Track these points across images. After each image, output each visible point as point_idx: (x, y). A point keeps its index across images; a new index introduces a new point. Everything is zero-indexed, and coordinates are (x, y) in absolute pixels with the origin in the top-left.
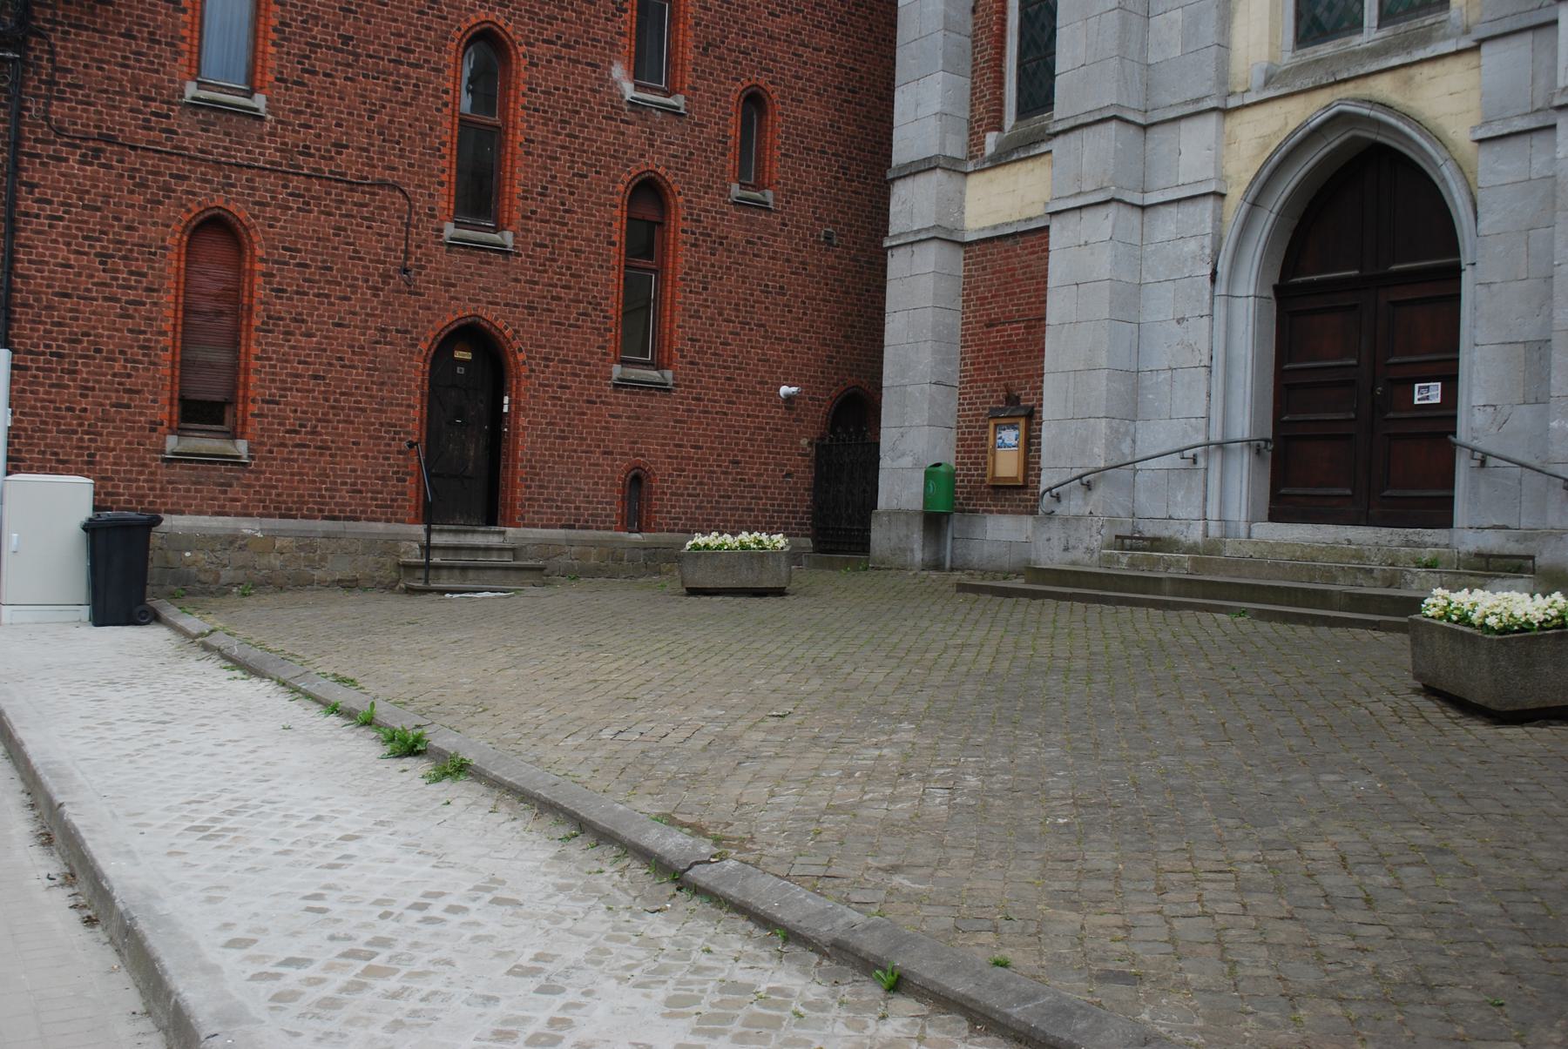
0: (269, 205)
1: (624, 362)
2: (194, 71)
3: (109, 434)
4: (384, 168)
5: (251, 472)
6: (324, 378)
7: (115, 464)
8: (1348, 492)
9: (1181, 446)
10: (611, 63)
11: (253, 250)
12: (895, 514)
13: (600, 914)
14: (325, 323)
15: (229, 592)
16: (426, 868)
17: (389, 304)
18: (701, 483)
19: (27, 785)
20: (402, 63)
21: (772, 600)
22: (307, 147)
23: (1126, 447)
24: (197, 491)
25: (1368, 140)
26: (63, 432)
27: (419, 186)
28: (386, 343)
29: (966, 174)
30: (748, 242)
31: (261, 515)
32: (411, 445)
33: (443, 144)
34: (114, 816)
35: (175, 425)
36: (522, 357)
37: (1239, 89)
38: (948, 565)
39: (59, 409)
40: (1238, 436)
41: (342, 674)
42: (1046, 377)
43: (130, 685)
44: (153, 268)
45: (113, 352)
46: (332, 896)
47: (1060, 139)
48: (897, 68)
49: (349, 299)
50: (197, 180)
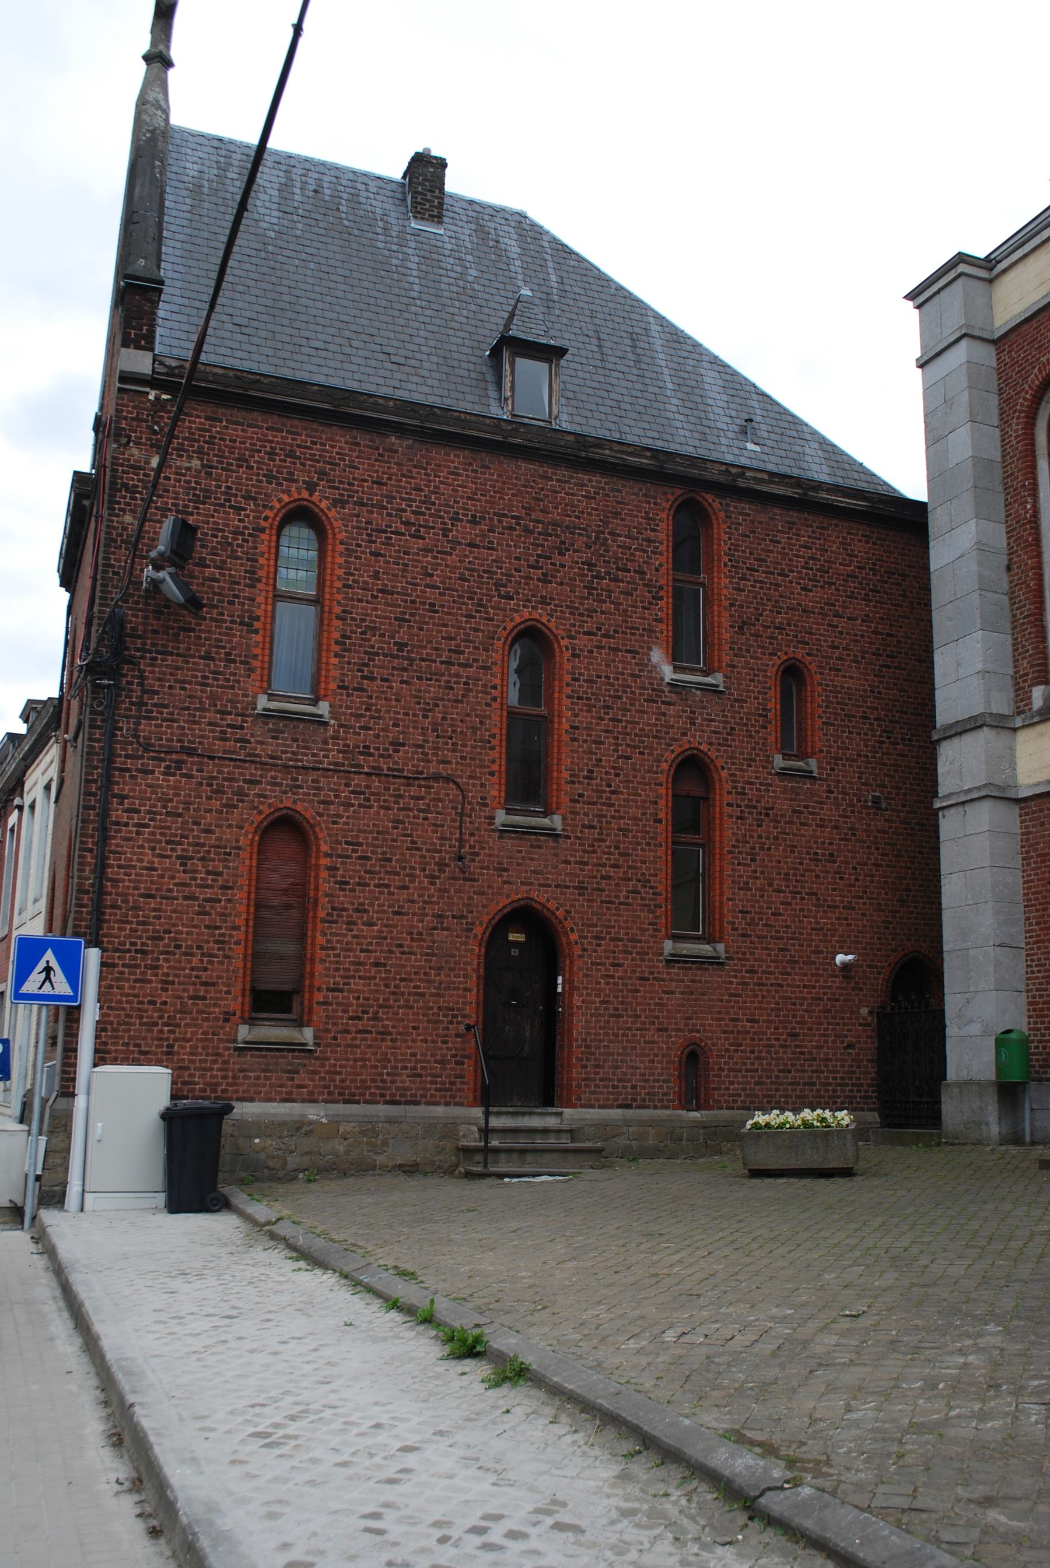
0: (332, 803)
1: (675, 938)
2: (265, 685)
3: (187, 1025)
4: (439, 762)
5: (317, 1058)
6: (385, 965)
7: (191, 1054)
10: (650, 649)
11: (318, 845)
12: (965, 1085)
13: (665, 1546)
14: (385, 912)
15: (295, 1178)
16: (486, 1486)
17: (445, 891)
18: (758, 1058)
19: (102, 1380)
20: (452, 664)
21: (840, 1181)
22: (368, 747)
24: (265, 1078)
26: (145, 1024)
27: (471, 777)
28: (443, 929)
29: (1015, 730)
30: (794, 811)
31: (326, 1101)
32: (469, 1028)
33: (493, 736)
34: (181, 1419)
35: (246, 1015)
36: (574, 937)
38: (1028, 1139)
39: (142, 1003)
41: (402, 1266)
43: (200, 1276)
44: (228, 867)
45: (191, 947)
46: (390, 1515)
48: (935, 631)
49: (407, 888)
50: (268, 784)
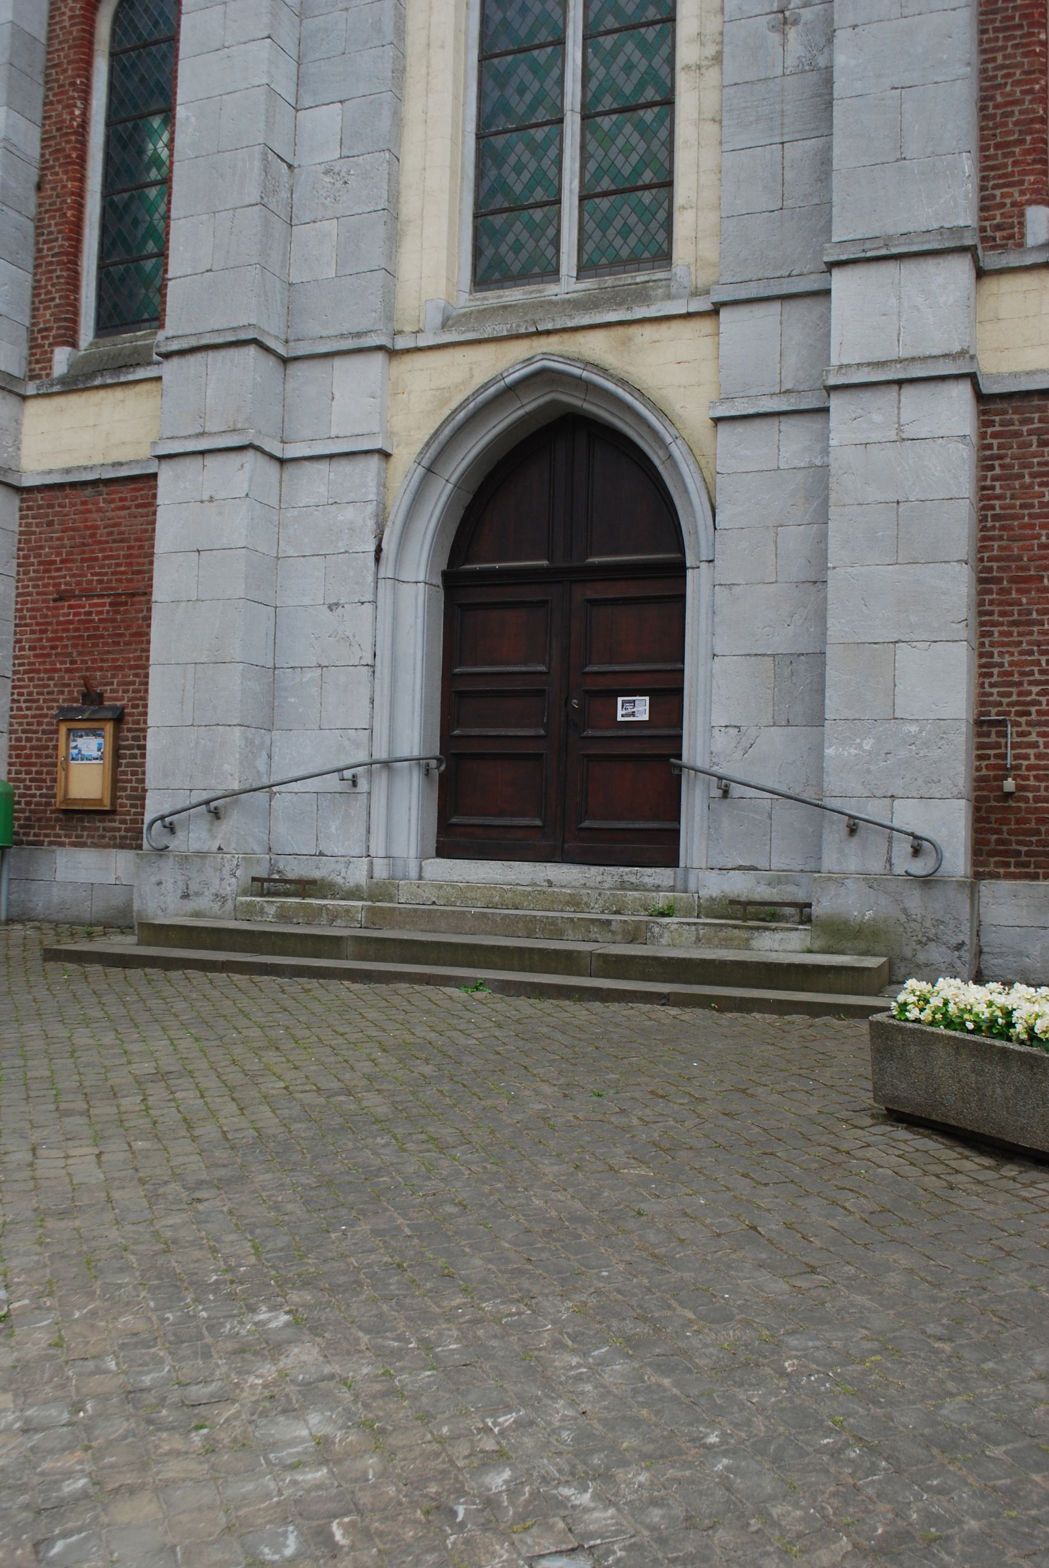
8: (538, 822)
9: (342, 764)
23: (261, 764)
25: (569, 405)
29: (24, 398)
37: (407, 329)
40: (406, 754)
42: (152, 670)
47: (175, 361)
